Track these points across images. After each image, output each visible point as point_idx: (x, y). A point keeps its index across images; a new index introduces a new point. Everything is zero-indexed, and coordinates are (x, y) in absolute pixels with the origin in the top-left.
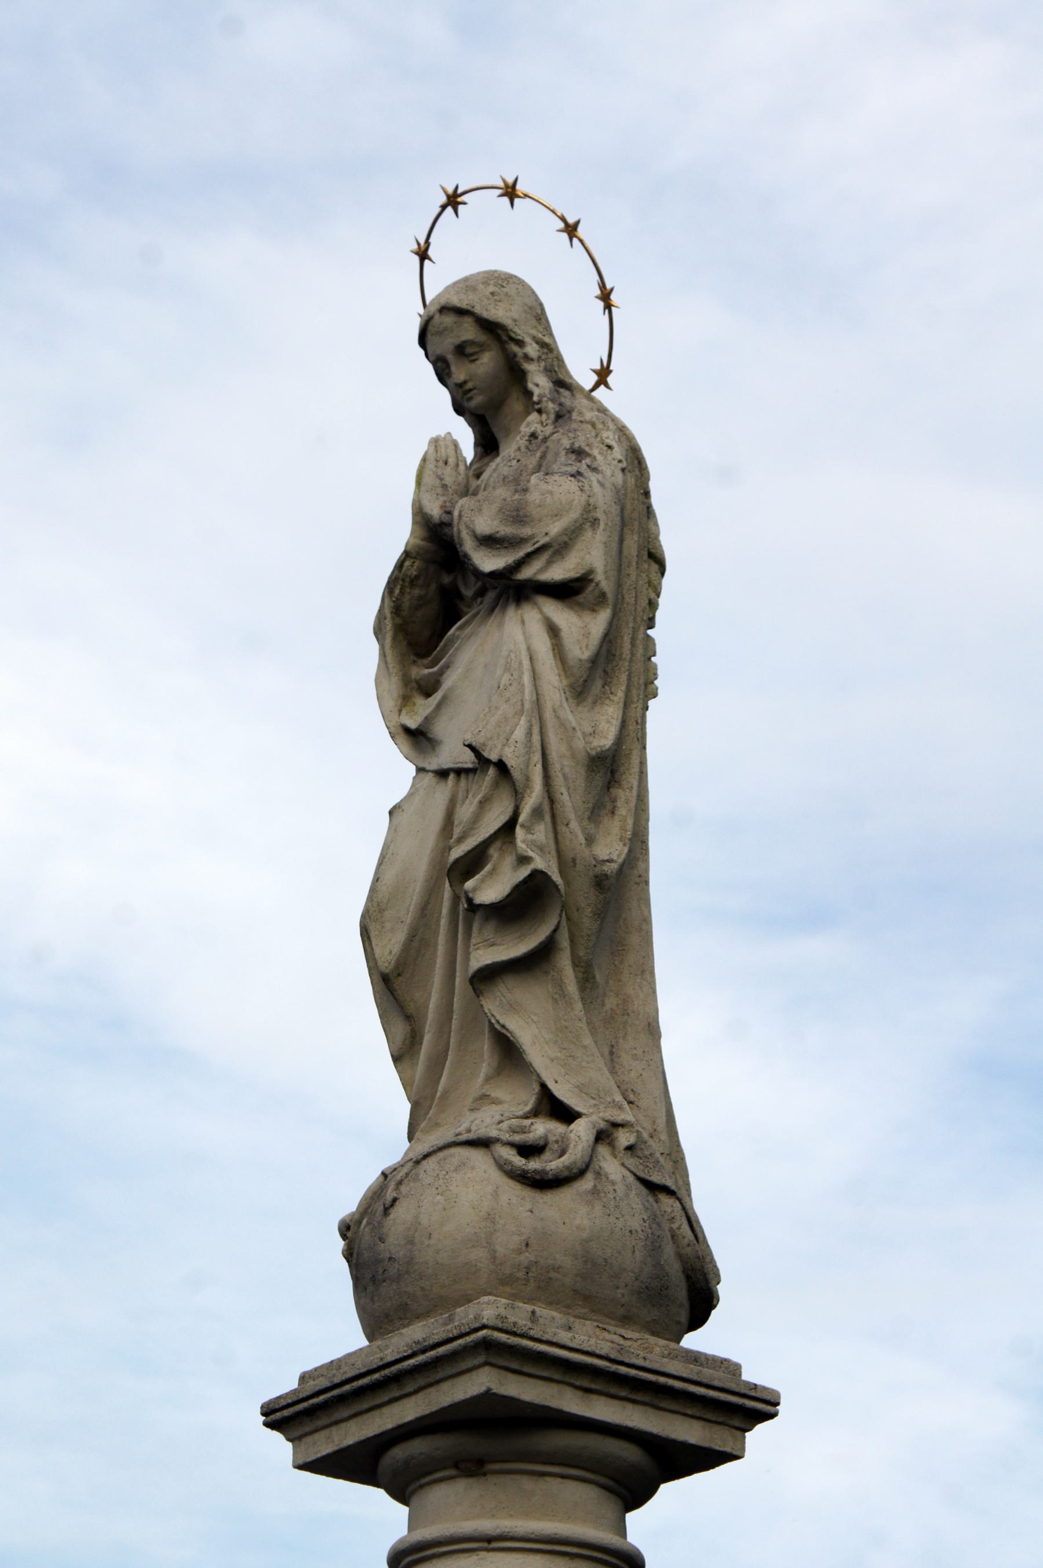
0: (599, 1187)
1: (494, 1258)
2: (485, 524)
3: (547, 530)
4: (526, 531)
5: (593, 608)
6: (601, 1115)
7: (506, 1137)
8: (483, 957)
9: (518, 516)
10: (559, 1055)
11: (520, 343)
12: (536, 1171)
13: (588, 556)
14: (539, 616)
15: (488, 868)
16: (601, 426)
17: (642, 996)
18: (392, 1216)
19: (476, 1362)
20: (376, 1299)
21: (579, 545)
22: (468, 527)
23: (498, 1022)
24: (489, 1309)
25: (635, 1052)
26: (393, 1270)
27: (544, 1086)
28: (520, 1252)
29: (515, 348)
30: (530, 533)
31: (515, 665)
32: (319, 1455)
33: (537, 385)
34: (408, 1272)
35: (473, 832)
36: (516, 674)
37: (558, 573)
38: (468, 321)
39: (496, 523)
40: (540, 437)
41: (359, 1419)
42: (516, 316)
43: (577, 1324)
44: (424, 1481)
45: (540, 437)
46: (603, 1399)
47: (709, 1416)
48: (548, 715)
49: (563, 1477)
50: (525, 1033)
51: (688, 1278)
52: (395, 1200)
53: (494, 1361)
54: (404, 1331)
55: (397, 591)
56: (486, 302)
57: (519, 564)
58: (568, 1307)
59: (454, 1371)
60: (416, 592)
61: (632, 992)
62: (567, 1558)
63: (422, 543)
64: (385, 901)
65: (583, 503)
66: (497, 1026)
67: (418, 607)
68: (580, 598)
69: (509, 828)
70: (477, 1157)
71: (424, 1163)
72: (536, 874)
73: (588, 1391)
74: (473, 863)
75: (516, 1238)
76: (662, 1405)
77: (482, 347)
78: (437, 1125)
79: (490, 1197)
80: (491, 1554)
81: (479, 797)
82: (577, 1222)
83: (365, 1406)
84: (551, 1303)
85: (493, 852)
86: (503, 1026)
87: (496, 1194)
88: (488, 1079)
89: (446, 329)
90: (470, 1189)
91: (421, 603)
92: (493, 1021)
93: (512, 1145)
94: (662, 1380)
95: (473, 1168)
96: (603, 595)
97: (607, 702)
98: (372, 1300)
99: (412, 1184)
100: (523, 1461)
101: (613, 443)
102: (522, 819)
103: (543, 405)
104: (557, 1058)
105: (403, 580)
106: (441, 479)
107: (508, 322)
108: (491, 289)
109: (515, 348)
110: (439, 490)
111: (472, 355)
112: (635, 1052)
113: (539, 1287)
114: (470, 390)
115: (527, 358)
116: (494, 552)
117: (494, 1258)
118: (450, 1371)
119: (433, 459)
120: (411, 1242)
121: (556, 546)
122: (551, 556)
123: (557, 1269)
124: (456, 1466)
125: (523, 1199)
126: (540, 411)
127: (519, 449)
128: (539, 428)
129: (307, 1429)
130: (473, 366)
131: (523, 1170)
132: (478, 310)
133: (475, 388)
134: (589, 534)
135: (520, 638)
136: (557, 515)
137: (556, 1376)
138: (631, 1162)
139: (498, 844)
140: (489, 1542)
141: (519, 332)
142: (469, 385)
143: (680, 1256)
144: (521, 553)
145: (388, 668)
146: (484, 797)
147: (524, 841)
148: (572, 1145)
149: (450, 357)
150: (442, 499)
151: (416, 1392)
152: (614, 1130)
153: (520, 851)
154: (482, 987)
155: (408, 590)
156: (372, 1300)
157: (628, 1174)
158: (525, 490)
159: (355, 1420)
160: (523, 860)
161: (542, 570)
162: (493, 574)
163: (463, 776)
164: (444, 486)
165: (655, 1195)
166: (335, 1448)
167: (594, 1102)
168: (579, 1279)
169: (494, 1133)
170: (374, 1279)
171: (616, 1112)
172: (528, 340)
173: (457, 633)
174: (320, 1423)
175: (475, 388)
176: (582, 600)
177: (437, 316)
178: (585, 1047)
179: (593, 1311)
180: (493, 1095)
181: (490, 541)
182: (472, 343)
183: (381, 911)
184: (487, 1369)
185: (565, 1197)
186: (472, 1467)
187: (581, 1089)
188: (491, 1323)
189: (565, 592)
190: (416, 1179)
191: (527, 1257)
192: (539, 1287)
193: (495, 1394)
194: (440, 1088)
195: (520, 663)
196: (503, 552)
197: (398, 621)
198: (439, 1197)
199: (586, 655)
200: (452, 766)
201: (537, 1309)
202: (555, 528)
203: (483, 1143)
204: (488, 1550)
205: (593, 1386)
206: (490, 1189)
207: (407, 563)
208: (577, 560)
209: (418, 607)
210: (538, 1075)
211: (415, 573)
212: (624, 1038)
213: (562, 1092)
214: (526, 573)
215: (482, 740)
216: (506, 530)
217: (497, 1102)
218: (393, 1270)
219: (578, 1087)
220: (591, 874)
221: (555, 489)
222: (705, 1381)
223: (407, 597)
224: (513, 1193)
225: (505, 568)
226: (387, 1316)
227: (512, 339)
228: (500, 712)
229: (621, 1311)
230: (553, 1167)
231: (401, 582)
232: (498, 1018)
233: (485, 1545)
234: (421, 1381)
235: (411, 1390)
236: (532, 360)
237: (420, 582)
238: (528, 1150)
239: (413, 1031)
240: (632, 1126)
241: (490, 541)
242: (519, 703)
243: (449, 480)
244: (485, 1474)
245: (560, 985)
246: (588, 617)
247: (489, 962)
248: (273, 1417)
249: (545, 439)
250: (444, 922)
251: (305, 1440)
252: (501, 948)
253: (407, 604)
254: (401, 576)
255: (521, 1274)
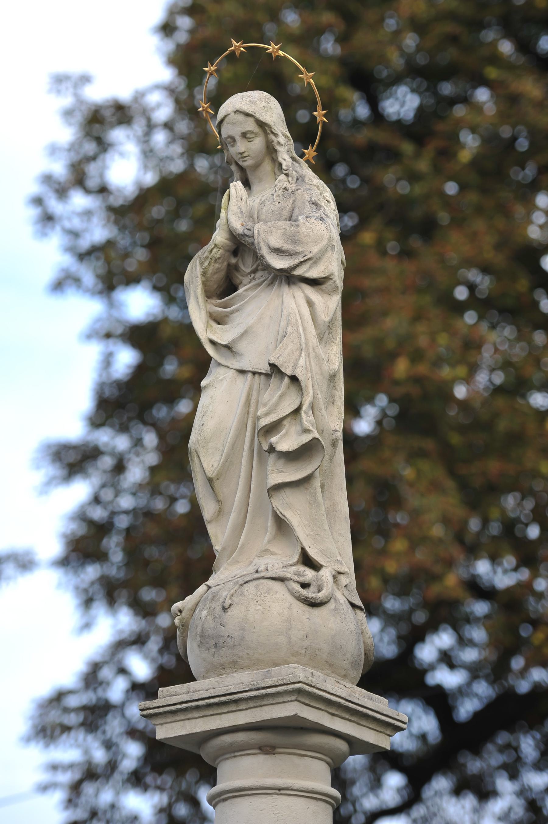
0: (337, 607)
1: (290, 642)
2: (276, 241)
3: (311, 249)
4: (299, 249)
5: (329, 294)
6: (333, 567)
7: (296, 578)
8: (276, 478)
9: (295, 240)
10: (311, 533)
11: (276, 135)
12: (312, 598)
13: (330, 266)
14: (302, 295)
15: (283, 432)
16: (322, 189)
17: (342, 501)
18: (229, 613)
19: (290, 699)
20: (216, 656)
21: (325, 259)
22: (264, 241)
23: (281, 513)
24: (299, 672)
25: (340, 532)
26: (230, 643)
27: (303, 549)
28: (303, 640)
29: (272, 137)
30: (301, 250)
31: (294, 322)
32: (176, 735)
33: (285, 160)
34: (240, 645)
35: (274, 411)
36: (295, 326)
37: (314, 273)
38: (251, 120)
39: (281, 241)
40: (290, 191)
41: (205, 718)
42: (275, 121)
43: (328, 679)
44: (236, 754)
45: (290, 191)
46: (338, 718)
47: (379, 729)
48: (311, 350)
49: (312, 757)
50: (293, 518)
51: (366, 654)
52: (231, 605)
53: (300, 699)
54: (235, 675)
55: (206, 264)
56: (261, 111)
57: (296, 267)
58: (322, 669)
59: (274, 702)
60: (217, 266)
61: (337, 499)
62: (315, 801)
63: (226, 241)
64: (209, 437)
65: (328, 237)
66: (280, 515)
67: (215, 274)
68: (323, 287)
69: (297, 411)
70: (277, 585)
71: (245, 585)
72: (315, 439)
73: (333, 715)
74: (274, 427)
75: (302, 633)
76: (361, 723)
77: (256, 135)
78: (237, 562)
79: (287, 609)
80: (279, 796)
81: (279, 393)
82: (330, 626)
83: (211, 712)
84: (315, 667)
85: (285, 422)
86: (284, 516)
87: (290, 608)
88: (269, 541)
89: (237, 123)
90: (277, 604)
91: (218, 270)
92: (278, 512)
93: (298, 582)
94: (365, 710)
95: (276, 592)
96: (337, 287)
97: (332, 343)
98: (213, 656)
99: (240, 597)
100: (295, 748)
101: (330, 200)
102: (304, 408)
103: (290, 172)
104: (310, 535)
105: (211, 259)
106: (240, 209)
107: (271, 123)
108: (264, 104)
109: (272, 137)
110: (240, 215)
111: (250, 138)
112: (340, 532)
113: (311, 659)
114: (246, 156)
115: (279, 143)
116: (280, 257)
117: (290, 642)
118: (271, 701)
119: (235, 196)
120: (243, 629)
121: (315, 259)
122: (312, 264)
123: (320, 650)
124: (260, 748)
125: (304, 612)
126: (287, 175)
127: (278, 196)
128: (288, 185)
129: (169, 720)
130: (249, 144)
131: (306, 597)
132: (258, 115)
133: (248, 156)
134: (329, 253)
135: (294, 306)
136: (316, 242)
137: (323, 708)
138: (346, 593)
139: (289, 419)
140: (279, 790)
141: (276, 129)
142: (245, 155)
143: (364, 643)
144: (297, 261)
145: (199, 305)
146: (282, 394)
147: (306, 421)
148: (325, 584)
149: (238, 138)
150: (241, 220)
151: (246, 709)
152: (338, 576)
153: (305, 426)
154: (273, 494)
155: (213, 264)
156: (213, 656)
157: (346, 600)
158: (298, 226)
159: (202, 719)
160: (306, 431)
161: (307, 271)
162: (280, 270)
163: (257, 376)
164: (242, 212)
165: (354, 611)
166: (188, 733)
167: (328, 560)
168: (329, 655)
169: (289, 576)
170: (216, 645)
171: (340, 566)
172: (280, 134)
173: (244, 293)
174: (178, 718)
175: (248, 156)
176: (324, 288)
177: (233, 114)
178: (325, 530)
179: (332, 672)
180: (271, 550)
181: (278, 251)
182: (252, 132)
183: (207, 442)
184: (296, 702)
185: (316, 611)
186: (268, 749)
187: (323, 552)
188: (303, 681)
189: (314, 283)
190: (242, 594)
191: (307, 643)
192: (311, 659)
193: (299, 716)
194: (240, 542)
195: (297, 321)
196: (285, 258)
197: (204, 279)
198: (259, 607)
199: (327, 319)
200: (251, 369)
201: (314, 671)
202: (316, 249)
203: (282, 580)
204: (278, 794)
205: (336, 713)
206: (287, 605)
207: (215, 250)
208: (324, 267)
209: (215, 274)
210: (301, 544)
211: (218, 256)
212: (334, 524)
213: (313, 553)
214: (298, 272)
215: (281, 362)
216: (287, 246)
217: (273, 554)
218: (230, 643)
219: (321, 551)
220: (331, 438)
221: (314, 227)
222: (381, 711)
223: (211, 268)
224: (300, 608)
225: (288, 268)
226: (222, 665)
227: (272, 132)
228: (289, 348)
229: (343, 673)
230: (320, 596)
231: (209, 260)
232: (281, 511)
233: (277, 792)
234: (251, 704)
235: (244, 708)
236: (282, 145)
237: (220, 261)
238: (305, 586)
239: (220, 508)
240: (348, 574)
241: (278, 251)
242: (299, 344)
243: (243, 209)
244: (274, 754)
245: (315, 497)
246: (326, 297)
247: (281, 481)
248: (145, 712)
249: (293, 192)
250: (245, 454)
251: (165, 725)
252: (286, 474)
253: (211, 271)
254: (210, 256)
255: (303, 652)
